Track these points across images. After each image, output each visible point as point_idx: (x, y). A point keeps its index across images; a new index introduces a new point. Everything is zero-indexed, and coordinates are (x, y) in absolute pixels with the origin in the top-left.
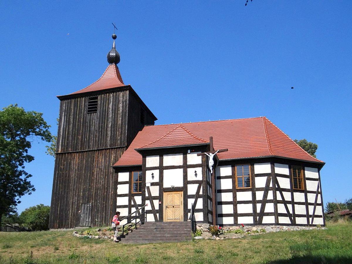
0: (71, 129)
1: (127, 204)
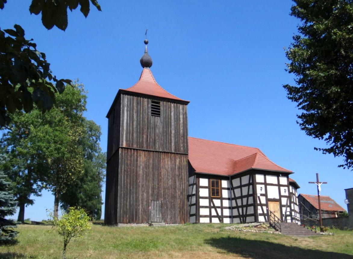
0: (135, 126)
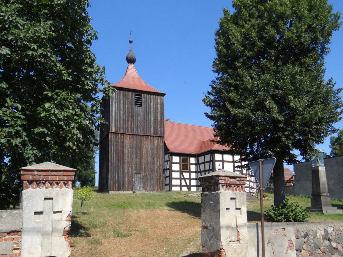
0: (121, 115)
1: (179, 177)
